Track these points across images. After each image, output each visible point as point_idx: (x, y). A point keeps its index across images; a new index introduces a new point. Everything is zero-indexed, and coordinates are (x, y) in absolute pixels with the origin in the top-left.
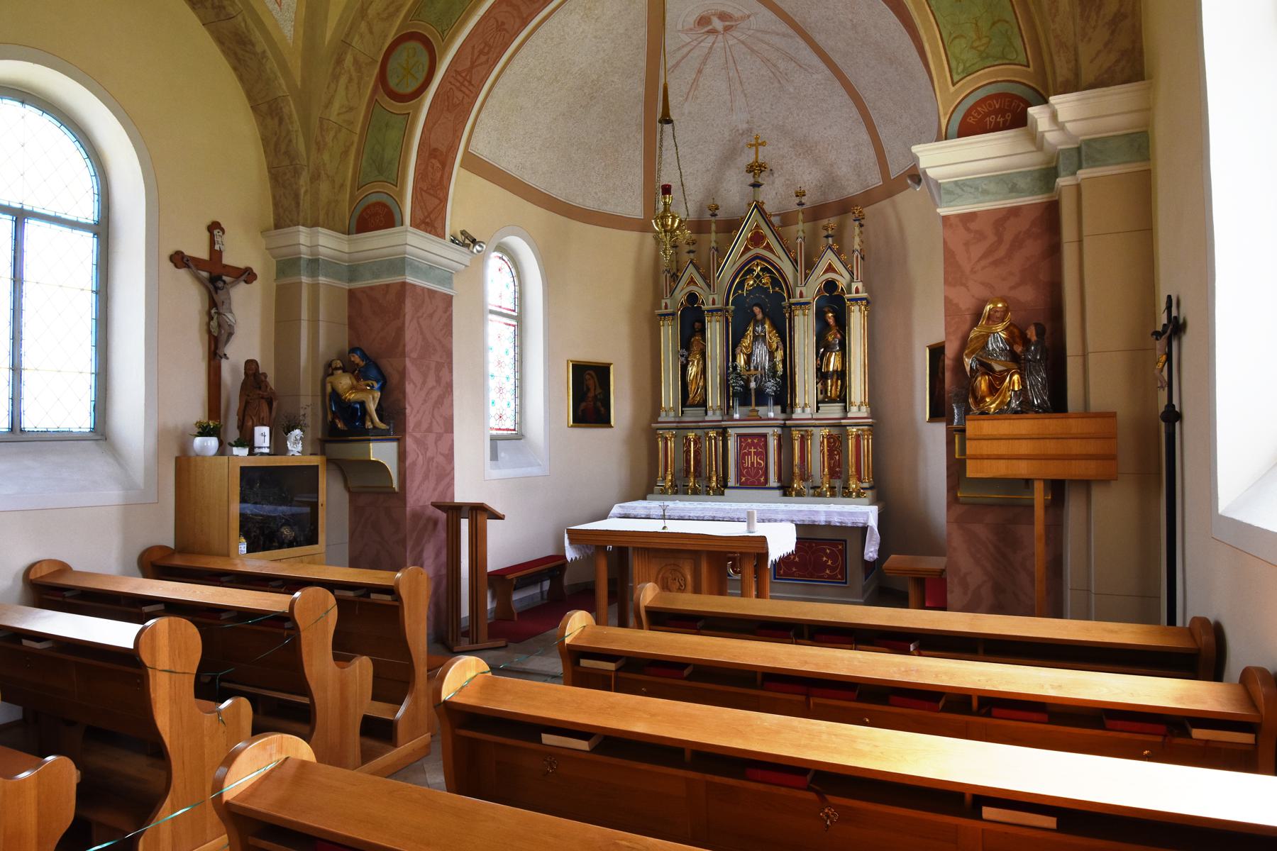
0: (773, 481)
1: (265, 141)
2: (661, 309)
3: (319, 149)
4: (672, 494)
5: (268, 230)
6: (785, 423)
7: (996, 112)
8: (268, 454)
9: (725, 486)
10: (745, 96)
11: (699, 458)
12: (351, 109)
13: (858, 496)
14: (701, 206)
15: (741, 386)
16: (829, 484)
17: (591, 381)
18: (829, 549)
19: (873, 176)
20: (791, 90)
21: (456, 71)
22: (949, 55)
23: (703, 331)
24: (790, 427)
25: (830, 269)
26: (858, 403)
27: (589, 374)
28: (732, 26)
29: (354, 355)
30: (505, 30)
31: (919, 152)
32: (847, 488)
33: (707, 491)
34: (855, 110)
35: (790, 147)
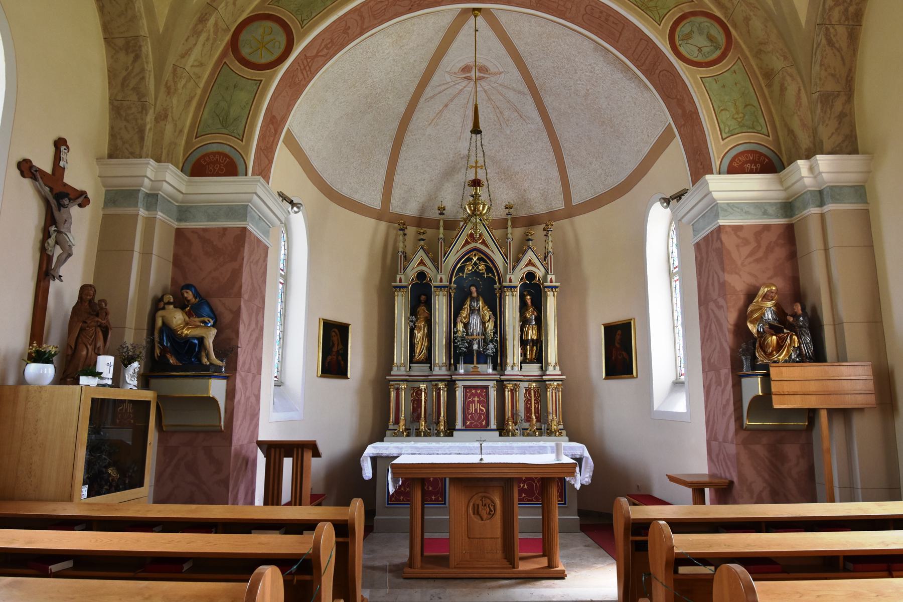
0: (493, 424)
1: (112, 74)
2: (396, 282)
3: (169, 93)
5: (101, 159)
7: (751, 162)
8: (110, 386)
12: (201, 65)
13: (560, 434)
14: (423, 207)
15: (466, 348)
17: (335, 334)
19: (558, 202)
20: (508, 132)
21: (305, 55)
22: (719, 120)
26: (553, 364)
27: (334, 331)
28: (484, 78)
29: (188, 291)
30: (348, 34)
31: (709, 179)
34: (552, 154)
35: (496, 173)
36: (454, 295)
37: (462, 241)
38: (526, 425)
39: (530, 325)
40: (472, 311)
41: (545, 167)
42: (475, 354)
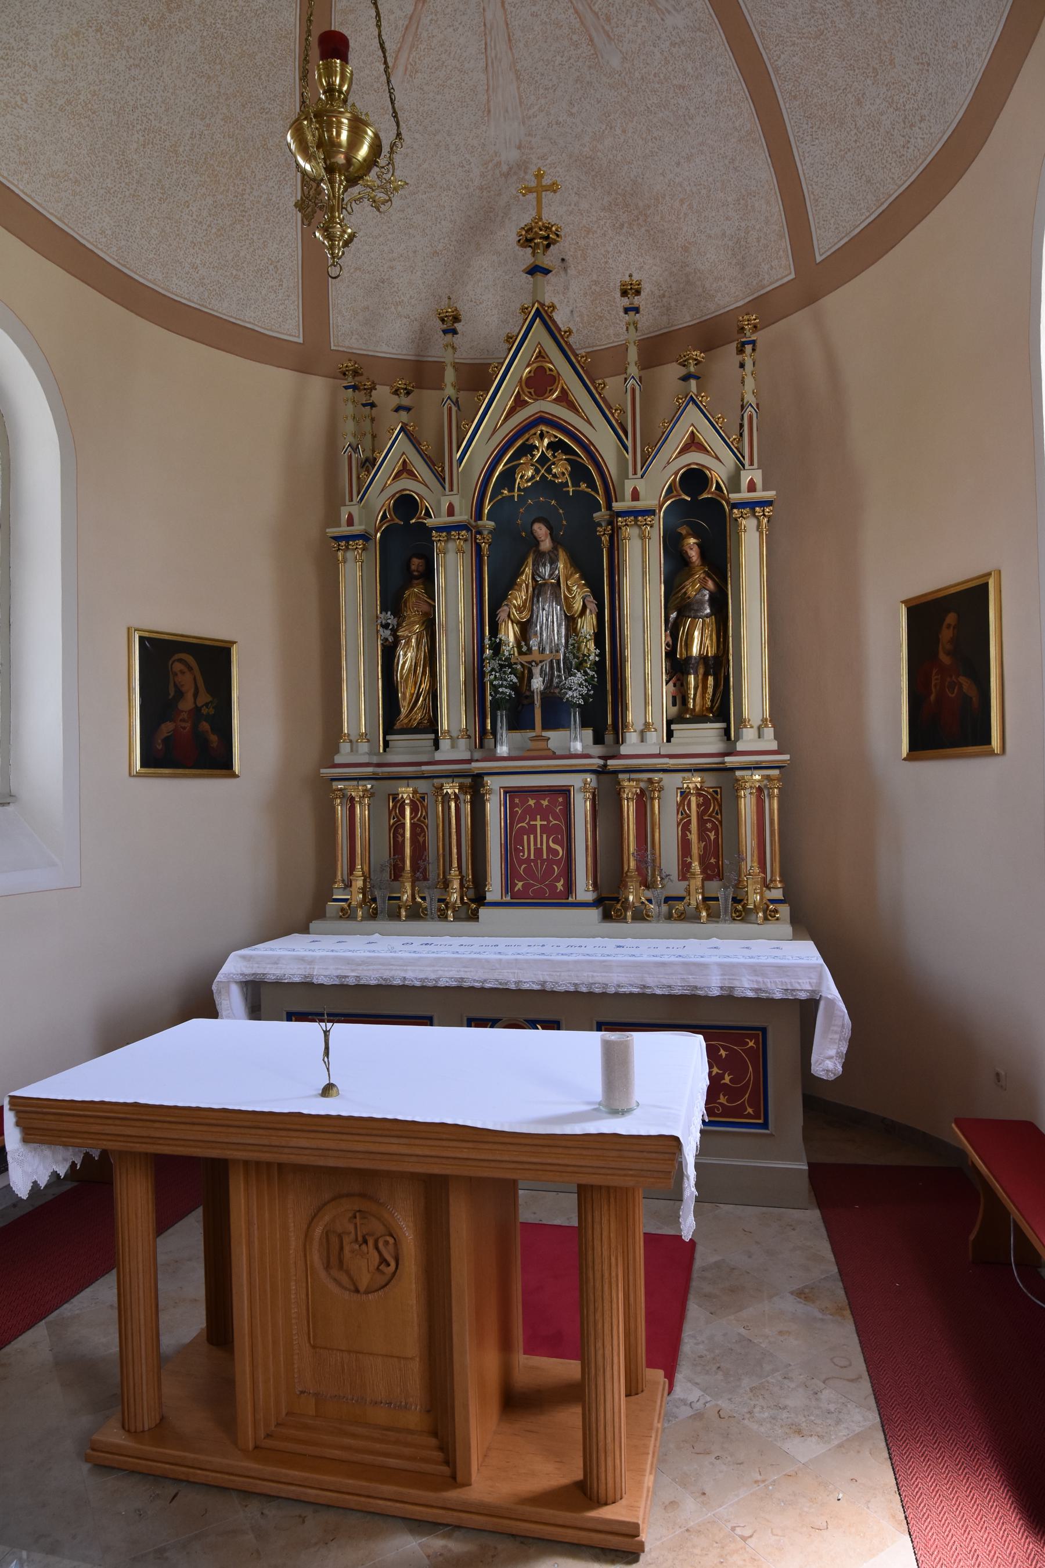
0: (584, 891)
4: (363, 919)
6: (605, 765)
9: (480, 900)
10: (518, 78)
11: (421, 839)
13: (770, 916)
14: (422, 331)
15: (513, 687)
16: (703, 894)
18: (725, 1048)
20: (615, 62)
23: (428, 576)
24: (616, 772)
25: (694, 443)
26: (756, 721)
27: (180, 660)
32: (739, 901)
33: (440, 910)
35: (603, 209)
36: (489, 549)
37: (504, 399)
38: (677, 888)
39: (695, 618)
40: (538, 590)
41: (733, 161)
42: (537, 703)
